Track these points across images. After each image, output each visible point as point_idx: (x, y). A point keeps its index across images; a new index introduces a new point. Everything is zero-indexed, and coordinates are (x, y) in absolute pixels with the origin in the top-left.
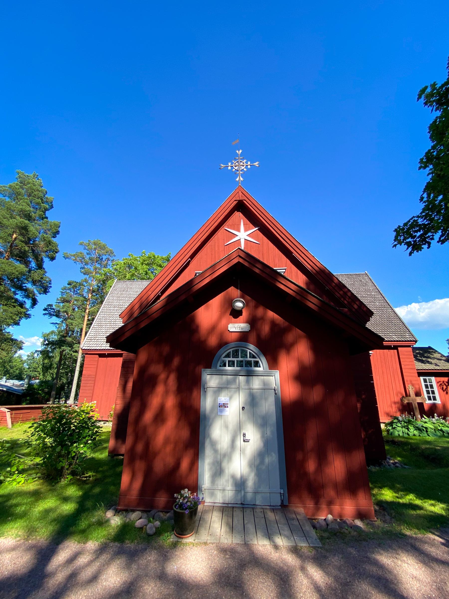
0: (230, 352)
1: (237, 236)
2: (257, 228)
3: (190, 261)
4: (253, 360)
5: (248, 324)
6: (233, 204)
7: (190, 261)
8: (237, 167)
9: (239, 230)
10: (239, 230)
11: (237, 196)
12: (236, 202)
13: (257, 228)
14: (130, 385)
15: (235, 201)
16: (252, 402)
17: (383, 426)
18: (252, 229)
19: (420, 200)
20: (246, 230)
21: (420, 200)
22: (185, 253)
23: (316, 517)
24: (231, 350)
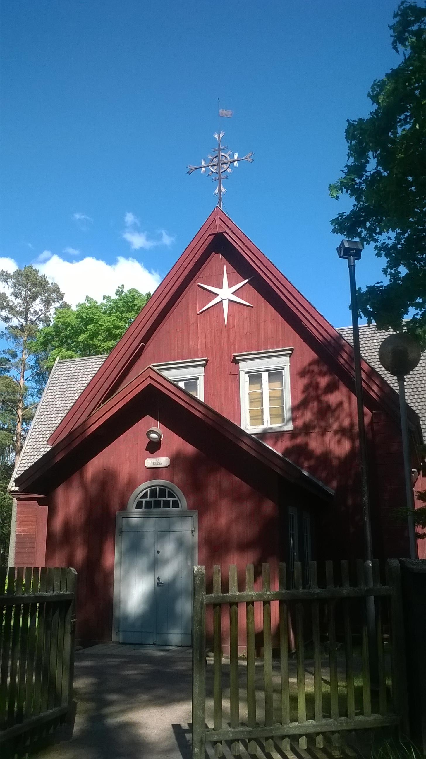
0: (147, 492)
1: (218, 295)
2: (247, 280)
3: (143, 347)
4: (171, 499)
5: (167, 458)
6: (203, 247)
7: (143, 347)
8: (216, 167)
9: (220, 286)
10: (220, 286)
11: (212, 227)
12: (211, 237)
13: (247, 280)
14: (403, 418)
15: (210, 235)
16: (180, 544)
17: (67, 593)
18: (243, 281)
19: (384, 274)
20: (230, 285)
21: (384, 274)
22: (135, 335)
23: (317, 650)
24: (148, 490)
